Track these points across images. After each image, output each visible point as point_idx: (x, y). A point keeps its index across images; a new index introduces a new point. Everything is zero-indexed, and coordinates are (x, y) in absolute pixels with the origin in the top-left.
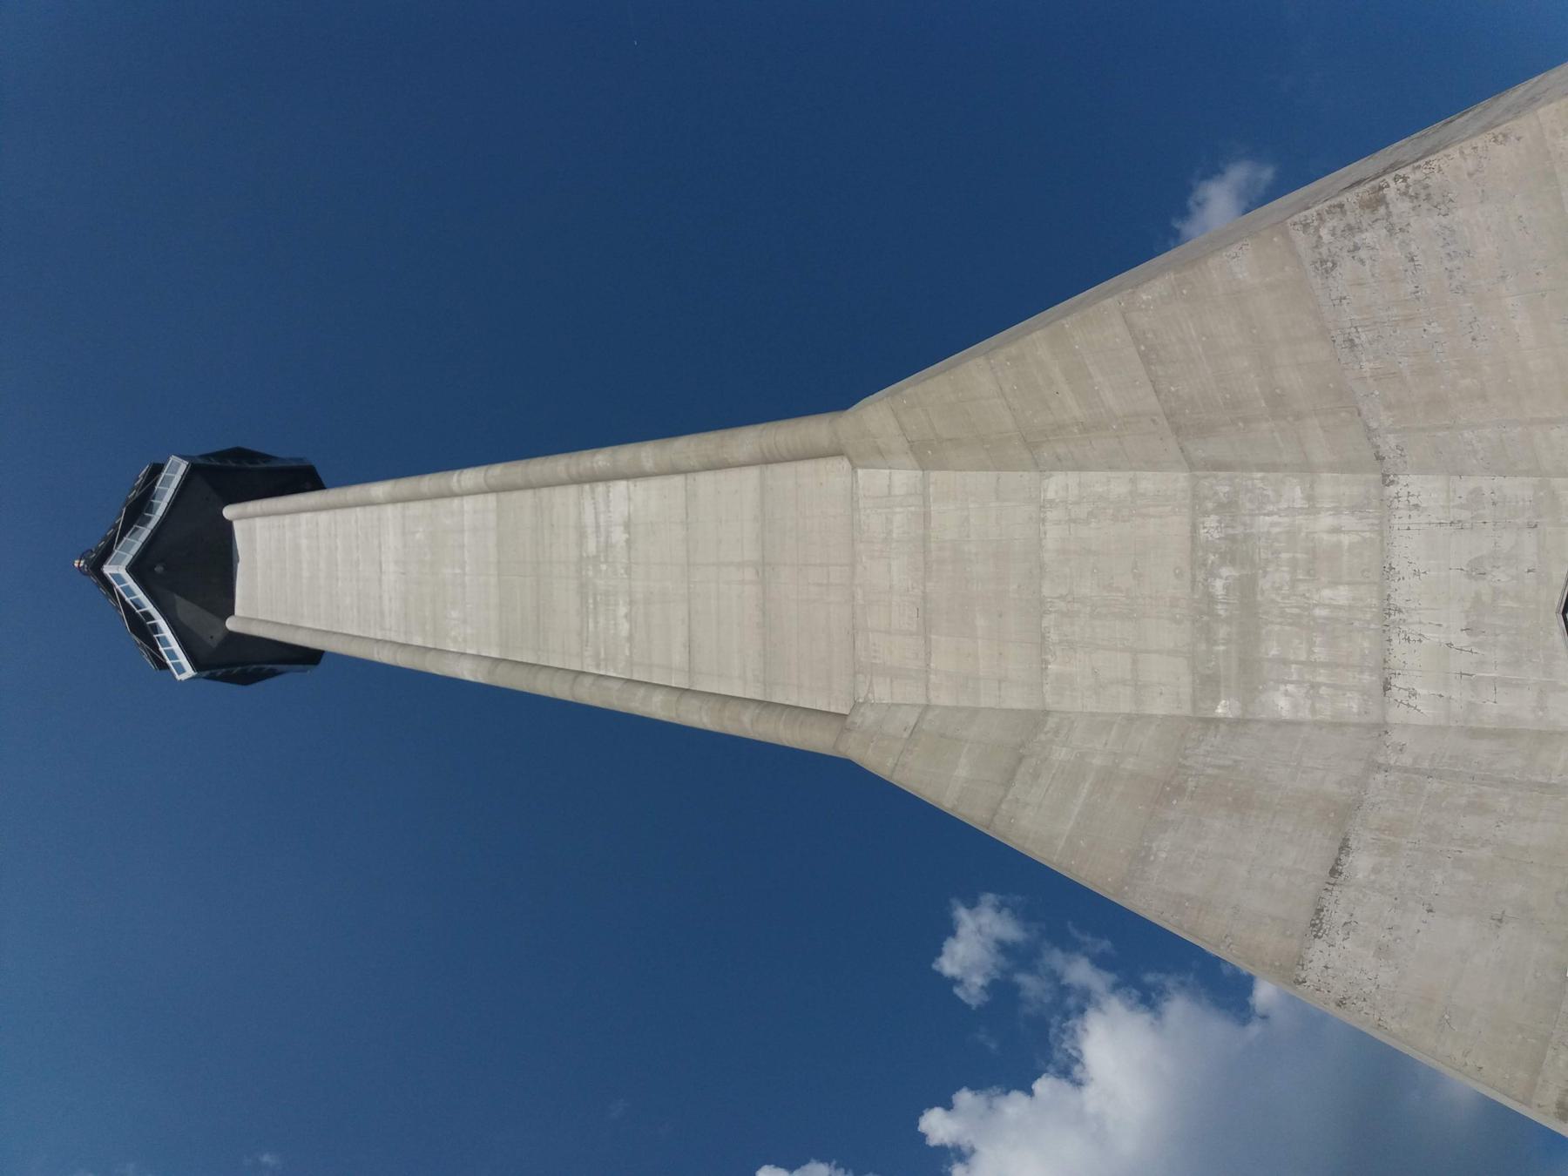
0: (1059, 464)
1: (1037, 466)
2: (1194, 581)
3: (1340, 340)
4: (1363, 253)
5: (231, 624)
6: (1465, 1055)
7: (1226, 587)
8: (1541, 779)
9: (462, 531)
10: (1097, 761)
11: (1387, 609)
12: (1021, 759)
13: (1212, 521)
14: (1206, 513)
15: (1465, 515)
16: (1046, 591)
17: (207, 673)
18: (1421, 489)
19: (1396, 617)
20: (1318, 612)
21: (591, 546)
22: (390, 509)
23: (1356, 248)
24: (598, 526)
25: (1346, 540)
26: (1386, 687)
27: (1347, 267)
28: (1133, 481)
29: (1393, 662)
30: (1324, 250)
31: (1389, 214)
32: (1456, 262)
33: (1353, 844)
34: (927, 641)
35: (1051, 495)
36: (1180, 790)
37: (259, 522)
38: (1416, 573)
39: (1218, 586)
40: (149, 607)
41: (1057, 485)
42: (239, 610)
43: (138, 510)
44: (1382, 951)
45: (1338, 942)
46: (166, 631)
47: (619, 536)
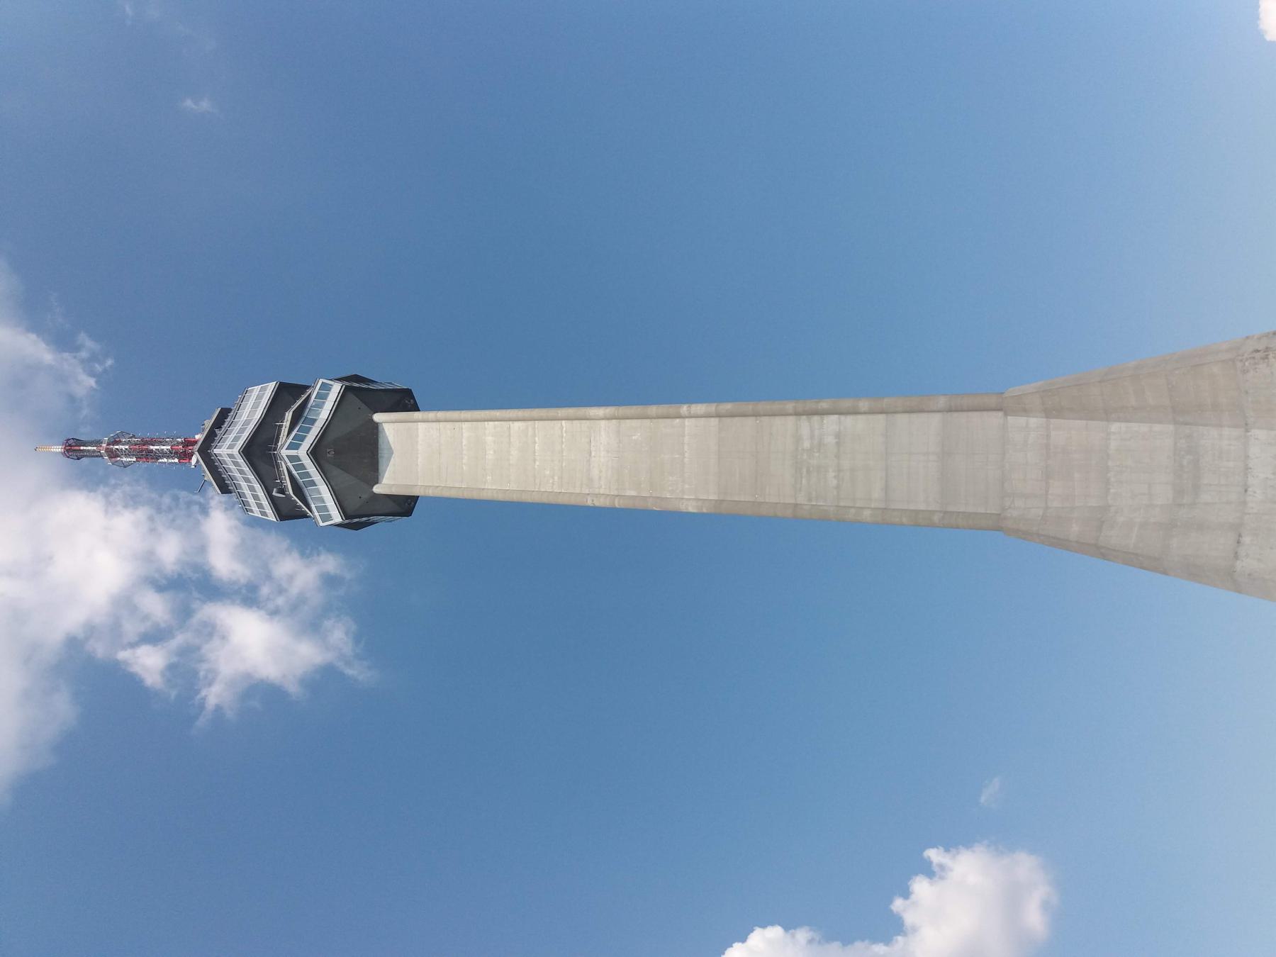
0: (1118, 420)
1: (1108, 420)
5: (377, 489)
11: (1247, 468)
18: (1259, 434)
22: (603, 423)
37: (465, 425)
41: (1115, 427)
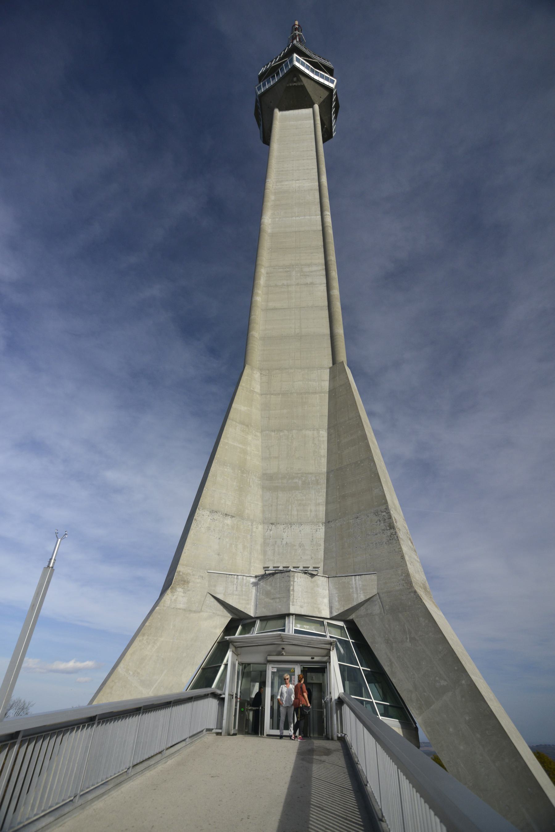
2: (298, 474)
3: (358, 515)
4: (378, 522)
6: (188, 550)
7: (296, 482)
8: (252, 561)
9: (310, 216)
10: (248, 449)
11: (291, 524)
12: (247, 426)
13: (314, 478)
14: (315, 477)
15: (314, 542)
16: (294, 431)
17: (258, 99)
19: (289, 526)
20: (290, 506)
21: (306, 269)
23: (380, 521)
24: (312, 272)
25: (309, 513)
26: (272, 524)
27: (376, 519)
28: (324, 456)
29: (278, 525)
30: (380, 513)
31: (387, 530)
32: (374, 545)
33: (233, 519)
34: (279, 394)
35: (321, 432)
36: (243, 472)
38: (300, 531)
39: (296, 480)
42: (281, 113)
44: (209, 528)
45: (210, 517)
47: (309, 280)
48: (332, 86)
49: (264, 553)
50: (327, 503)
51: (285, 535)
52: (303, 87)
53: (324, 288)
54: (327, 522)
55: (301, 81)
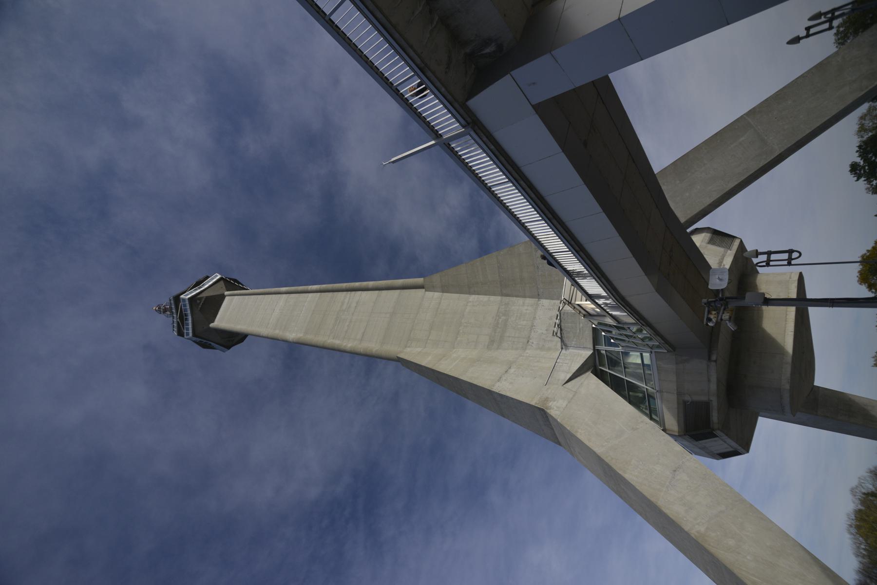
0: (475, 293)
5: (212, 325)
11: (533, 326)
17: (198, 340)
21: (344, 307)
40: (189, 312)
41: (473, 298)
43: (198, 284)
46: (190, 321)
47: (354, 305)
48: (219, 277)
49: (549, 349)
50: (524, 296)
51: (540, 331)
52: (207, 298)
53: (364, 293)
54: (538, 296)
55: (201, 298)
